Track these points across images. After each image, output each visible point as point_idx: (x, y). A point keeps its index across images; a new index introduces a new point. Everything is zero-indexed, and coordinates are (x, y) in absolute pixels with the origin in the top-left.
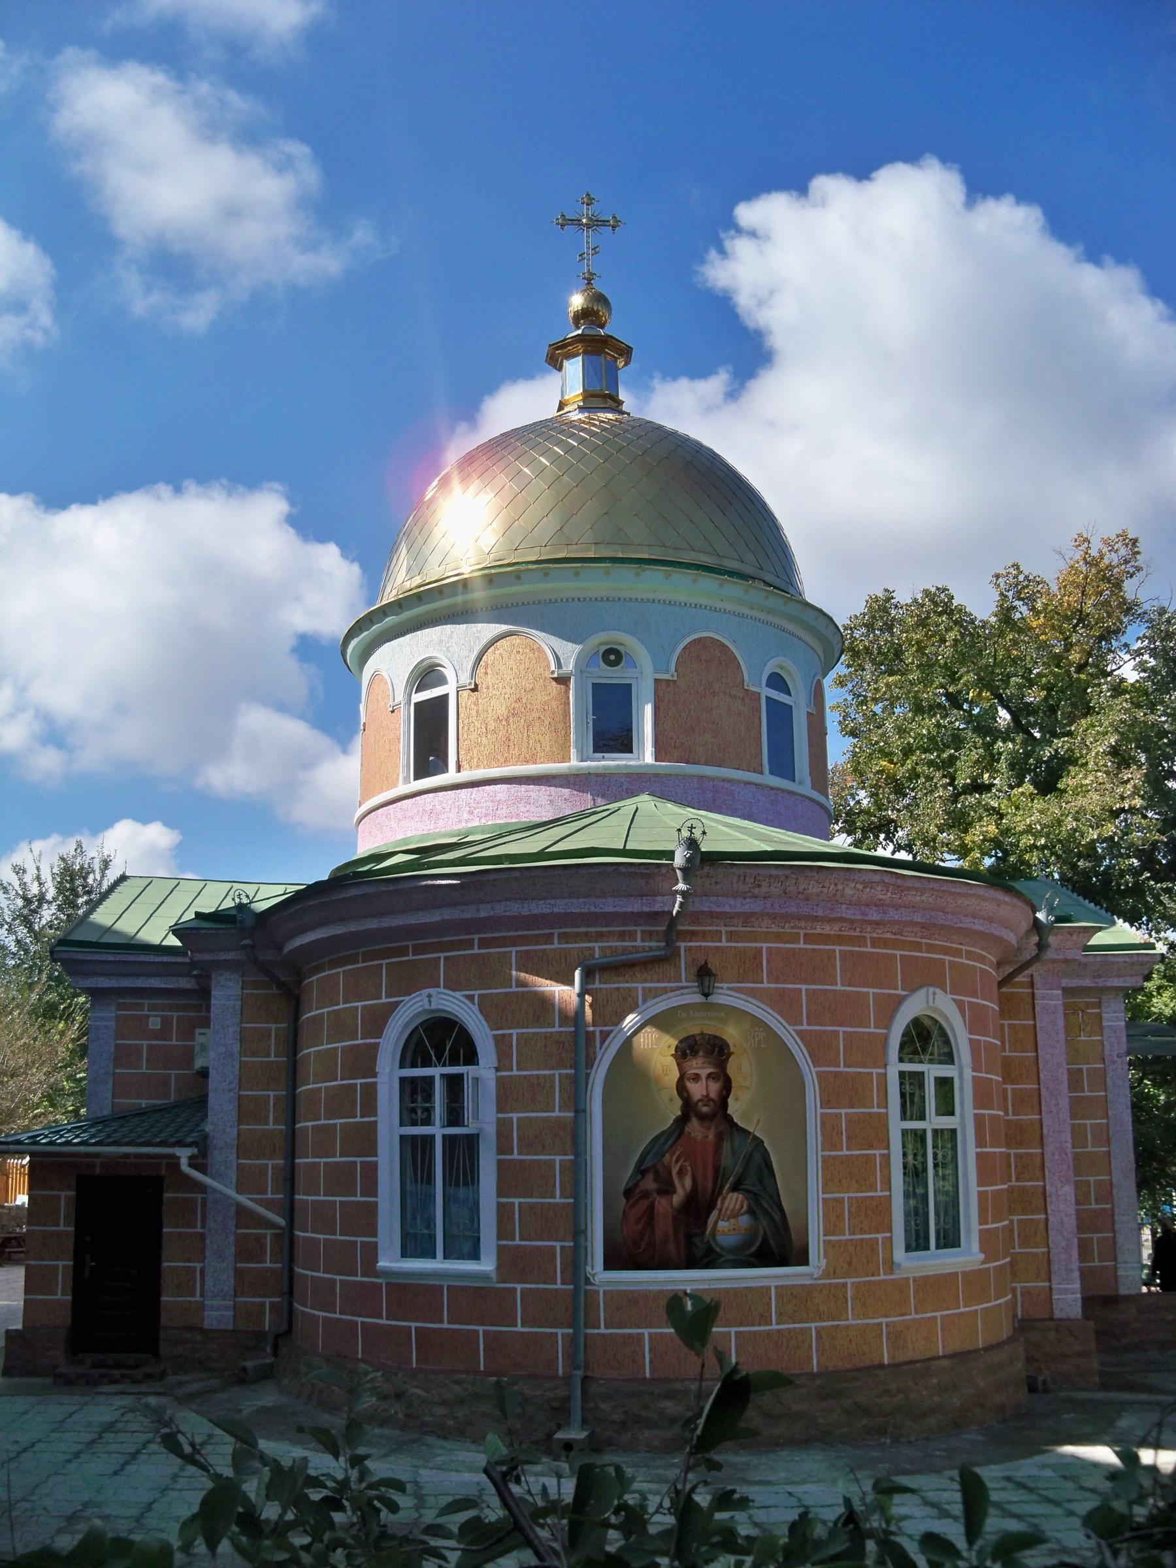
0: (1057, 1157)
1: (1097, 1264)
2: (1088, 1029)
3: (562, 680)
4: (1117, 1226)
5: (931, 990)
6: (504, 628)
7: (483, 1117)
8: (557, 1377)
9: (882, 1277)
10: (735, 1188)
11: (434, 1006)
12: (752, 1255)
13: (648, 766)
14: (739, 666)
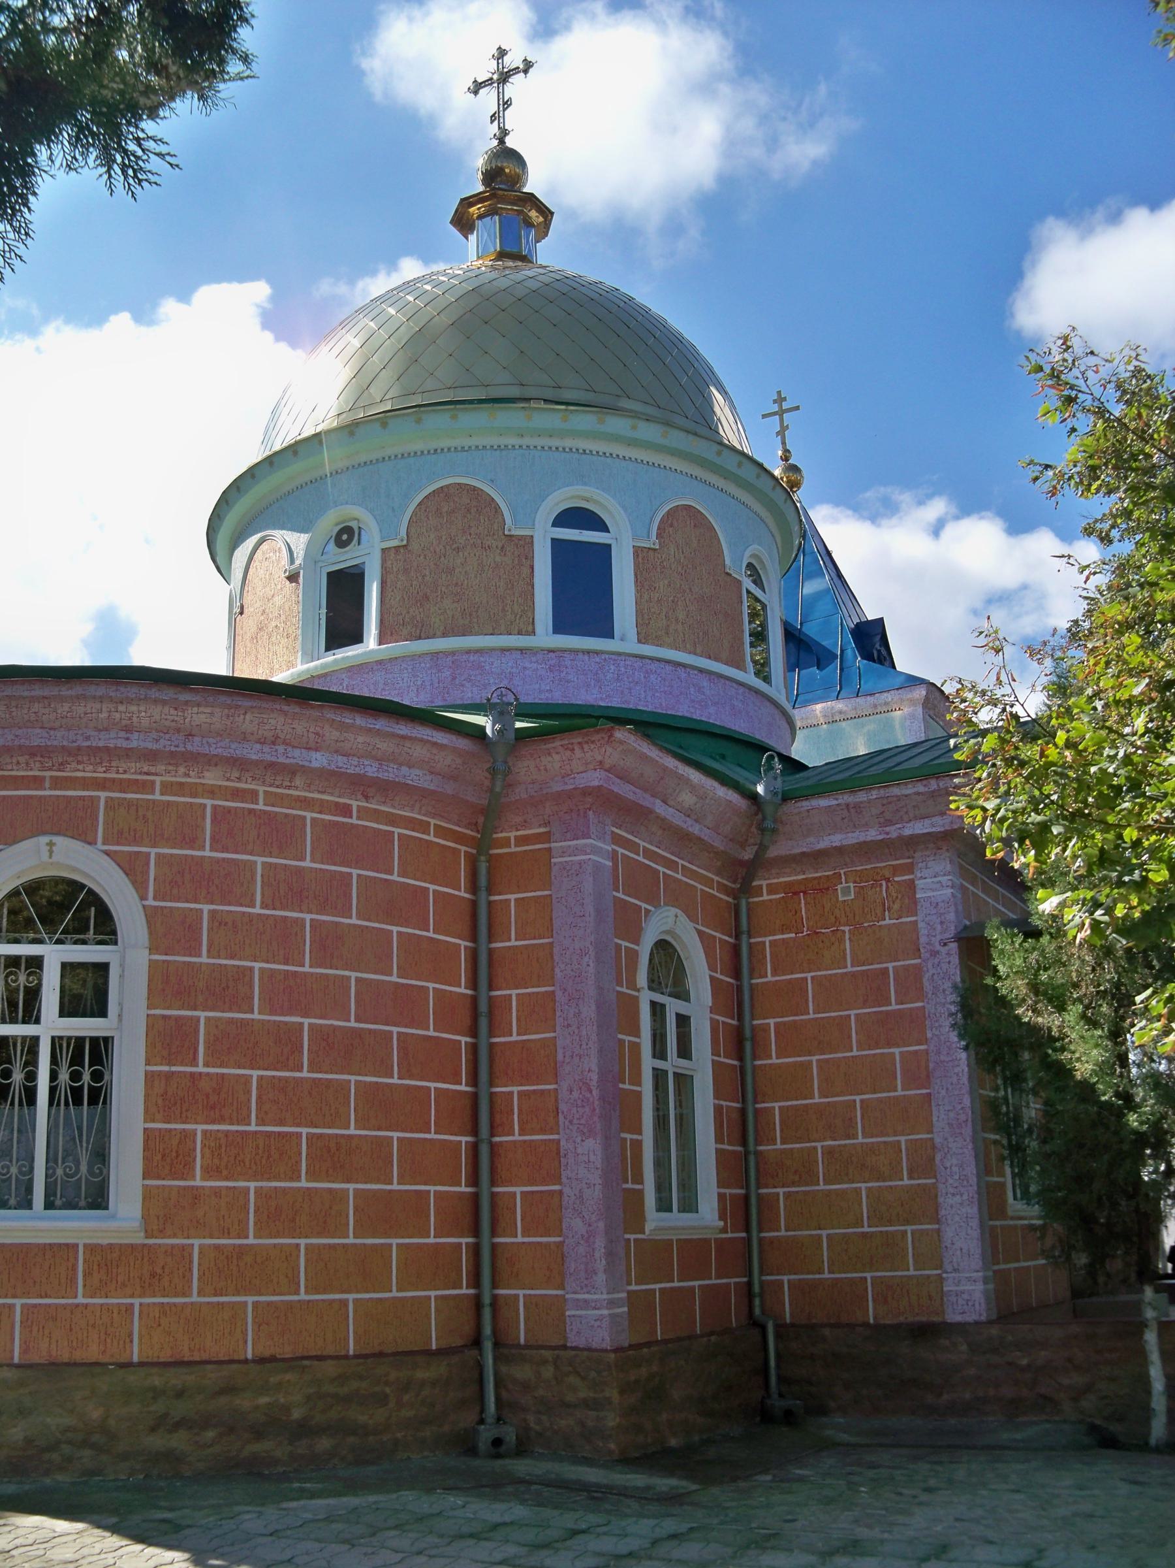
0: (576, 1094)
1: (912, 1272)
2: (896, 906)
3: (293, 578)
5: (44, 840)
6: (259, 536)
7: (127, 1022)
13: (372, 651)
14: (497, 509)
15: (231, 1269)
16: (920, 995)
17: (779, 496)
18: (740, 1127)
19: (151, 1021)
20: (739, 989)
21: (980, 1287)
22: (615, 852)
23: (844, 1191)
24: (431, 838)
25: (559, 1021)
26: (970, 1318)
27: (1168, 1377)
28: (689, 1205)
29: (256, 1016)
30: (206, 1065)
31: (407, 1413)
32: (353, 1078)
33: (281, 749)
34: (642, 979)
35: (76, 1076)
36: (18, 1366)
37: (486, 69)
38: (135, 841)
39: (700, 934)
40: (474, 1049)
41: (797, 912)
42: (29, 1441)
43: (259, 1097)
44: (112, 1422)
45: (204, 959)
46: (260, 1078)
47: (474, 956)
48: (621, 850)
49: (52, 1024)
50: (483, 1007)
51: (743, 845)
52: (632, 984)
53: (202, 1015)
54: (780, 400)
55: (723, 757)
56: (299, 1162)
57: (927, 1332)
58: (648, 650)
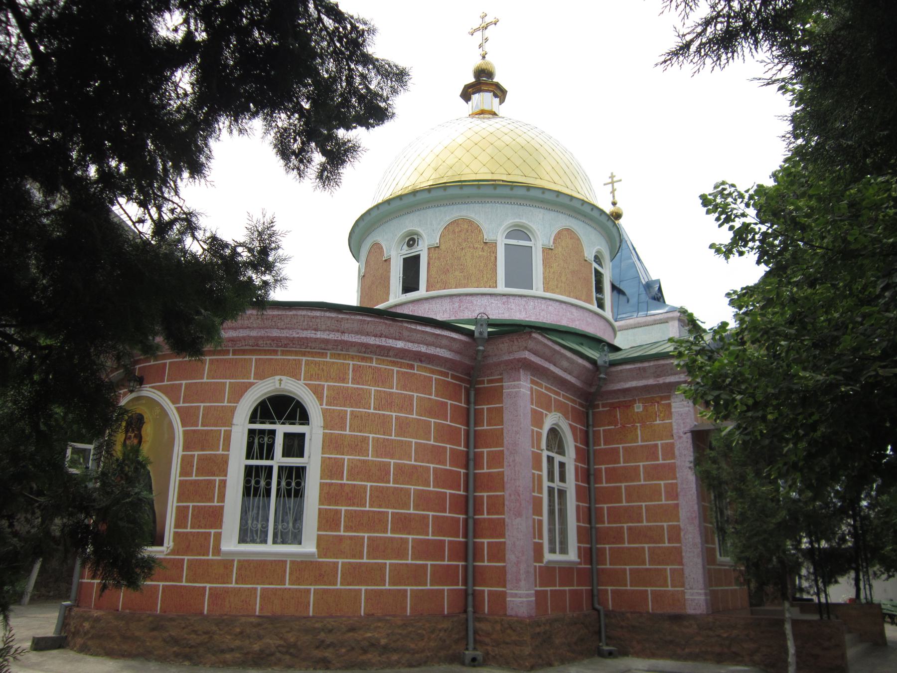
0: (513, 497)
4: (685, 560)
5: (278, 378)
7: (313, 459)
8: (202, 613)
9: (210, 557)
11: (282, 386)
15: (356, 574)
16: (673, 457)
17: (610, 224)
18: (588, 515)
19: (324, 460)
20: (588, 451)
21: (703, 598)
22: (532, 388)
23: (637, 548)
24: (449, 380)
25: (505, 464)
26: (698, 612)
27: (797, 647)
28: (564, 550)
29: (370, 458)
30: (347, 480)
31: (432, 644)
32: (412, 487)
33: (384, 339)
34: (544, 445)
35: (289, 484)
36: (259, 616)
37: (477, 23)
38: (318, 379)
39: (570, 425)
40: (467, 475)
41: (615, 416)
42: (262, 651)
43: (371, 495)
44: (299, 643)
45: (347, 432)
46: (371, 486)
47: (467, 433)
48: (534, 387)
49: (279, 460)
50: (471, 456)
51: (591, 385)
52: (539, 448)
53: (346, 457)
54: (612, 177)
55: (582, 344)
56: (387, 525)
57: (678, 618)
58: (548, 295)
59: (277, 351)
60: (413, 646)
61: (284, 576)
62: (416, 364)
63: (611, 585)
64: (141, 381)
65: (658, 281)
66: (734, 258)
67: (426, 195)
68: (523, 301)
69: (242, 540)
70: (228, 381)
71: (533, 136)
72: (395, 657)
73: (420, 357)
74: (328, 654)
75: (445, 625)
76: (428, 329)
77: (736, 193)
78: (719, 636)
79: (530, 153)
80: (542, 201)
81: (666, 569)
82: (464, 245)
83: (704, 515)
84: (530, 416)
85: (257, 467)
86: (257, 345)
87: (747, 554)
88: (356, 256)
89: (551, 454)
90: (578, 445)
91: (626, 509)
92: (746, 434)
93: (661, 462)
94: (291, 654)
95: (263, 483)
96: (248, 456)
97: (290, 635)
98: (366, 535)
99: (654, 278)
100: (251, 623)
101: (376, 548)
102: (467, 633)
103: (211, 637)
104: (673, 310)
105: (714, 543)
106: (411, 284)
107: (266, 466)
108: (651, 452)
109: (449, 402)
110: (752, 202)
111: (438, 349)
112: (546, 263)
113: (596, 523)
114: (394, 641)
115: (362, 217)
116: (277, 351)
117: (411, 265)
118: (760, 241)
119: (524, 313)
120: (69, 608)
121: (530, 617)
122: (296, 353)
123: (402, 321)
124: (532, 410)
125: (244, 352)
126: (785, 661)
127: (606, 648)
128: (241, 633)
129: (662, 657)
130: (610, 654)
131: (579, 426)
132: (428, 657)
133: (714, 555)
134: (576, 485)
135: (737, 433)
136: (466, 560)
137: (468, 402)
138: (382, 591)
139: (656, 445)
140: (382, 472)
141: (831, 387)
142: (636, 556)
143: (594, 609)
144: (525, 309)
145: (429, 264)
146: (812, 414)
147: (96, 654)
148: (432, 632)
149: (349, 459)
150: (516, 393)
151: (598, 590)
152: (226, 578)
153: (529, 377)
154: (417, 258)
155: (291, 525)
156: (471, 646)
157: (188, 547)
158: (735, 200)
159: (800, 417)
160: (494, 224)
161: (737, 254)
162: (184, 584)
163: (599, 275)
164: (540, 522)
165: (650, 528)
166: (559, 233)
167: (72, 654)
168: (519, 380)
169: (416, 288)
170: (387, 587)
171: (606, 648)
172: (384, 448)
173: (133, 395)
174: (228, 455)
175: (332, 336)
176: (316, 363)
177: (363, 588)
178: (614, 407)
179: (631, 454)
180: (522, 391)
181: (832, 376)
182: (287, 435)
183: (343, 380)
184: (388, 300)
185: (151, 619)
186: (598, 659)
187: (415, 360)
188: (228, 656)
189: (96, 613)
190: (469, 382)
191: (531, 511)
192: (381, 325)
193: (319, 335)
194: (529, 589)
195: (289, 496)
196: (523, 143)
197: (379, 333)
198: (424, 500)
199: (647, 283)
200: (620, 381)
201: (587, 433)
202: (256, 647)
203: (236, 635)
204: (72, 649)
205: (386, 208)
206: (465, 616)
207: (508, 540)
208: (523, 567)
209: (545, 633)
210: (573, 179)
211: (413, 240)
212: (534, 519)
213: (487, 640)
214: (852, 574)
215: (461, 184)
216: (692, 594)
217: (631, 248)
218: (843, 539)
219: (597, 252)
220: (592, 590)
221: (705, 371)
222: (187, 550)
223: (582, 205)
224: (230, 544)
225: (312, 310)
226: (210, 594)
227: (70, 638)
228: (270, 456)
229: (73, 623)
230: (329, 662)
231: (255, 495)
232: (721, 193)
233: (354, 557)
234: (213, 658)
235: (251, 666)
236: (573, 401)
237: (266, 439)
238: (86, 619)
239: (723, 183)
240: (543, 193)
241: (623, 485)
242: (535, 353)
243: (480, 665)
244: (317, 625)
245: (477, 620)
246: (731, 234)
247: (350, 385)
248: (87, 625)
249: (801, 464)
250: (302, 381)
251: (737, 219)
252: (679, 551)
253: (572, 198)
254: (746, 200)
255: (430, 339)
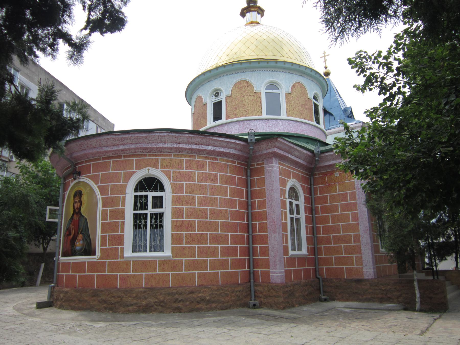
4: (362, 252)
5: (147, 168)
7: (167, 209)
8: (116, 288)
9: (119, 260)
10: (81, 233)
11: (150, 173)
12: (83, 252)
15: (192, 265)
18: (313, 231)
19: (173, 209)
20: (311, 198)
21: (372, 270)
22: (279, 167)
23: (338, 246)
24: (236, 165)
25: (267, 206)
26: (370, 278)
28: (300, 249)
29: (197, 207)
30: (185, 218)
31: (233, 298)
33: (200, 146)
34: (287, 196)
35: (156, 222)
38: (168, 168)
39: (301, 185)
40: (248, 213)
42: (147, 305)
43: (198, 226)
44: (165, 300)
45: (184, 194)
46: (198, 221)
49: (150, 210)
50: (250, 203)
51: (311, 164)
52: (284, 197)
54: (324, 53)
55: (308, 143)
57: (359, 281)
59: (146, 155)
60: (223, 300)
61: (156, 268)
62: (218, 158)
63: (325, 266)
64: (79, 174)
65: (350, 108)
66: (367, 92)
67: (223, 69)
68: (276, 122)
69: (134, 251)
70: (122, 171)
71: (279, 34)
72: (214, 305)
73: (220, 154)
74: (180, 305)
75: (239, 289)
76: (223, 139)
77: (367, 57)
78: (381, 289)
79: (277, 43)
80: (284, 68)
81: (353, 257)
82: (244, 94)
83: (372, 228)
84: (279, 182)
85: (140, 214)
86: (136, 152)
87: (393, 248)
88: (190, 103)
89: (291, 200)
90: (306, 195)
91: (332, 227)
92: (372, 187)
93: (349, 202)
94: (161, 306)
95: (143, 222)
96: (135, 210)
97: (160, 297)
98: (196, 246)
99: (348, 106)
100: (141, 291)
101: (202, 252)
102: (251, 293)
103: (122, 299)
104: (359, 122)
105: (378, 242)
106: (218, 116)
107: (144, 214)
108: (344, 197)
109: (237, 176)
110: (376, 61)
111: (229, 149)
112: (287, 101)
113: (317, 235)
114: (213, 298)
115: (191, 83)
116: (146, 155)
117: (217, 106)
118: (380, 82)
119: (277, 128)
120: (53, 287)
121: (282, 283)
122: (156, 155)
123: (209, 136)
124: (280, 178)
125: (129, 156)
126: (415, 301)
127: (323, 297)
128: (136, 296)
129: (352, 300)
130: (325, 300)
131: (306, 185)
132: (231, 305)
133: (379, 249)
134: (305, 216)
135: (368, 186)
136: (249, 256)
137: (247, 175)
138: (206, 273)
139: (347, 193)
140: (203, 214)
141: (416, 160)
142: (337, 251)
143: (317, 278)
144: (277, 126)
145: (226, 105)
146: (407, 174)
147: (67, 309)
148: (233, 292)
149: (186, 208)
150: (271, 170)
151: (319, 268)
152: (127, 270)
153: (278, 161)
154: (220, 102)
155: (158, 242)
156: (253, 298)
157: (108, 255)
158: (367, 60)
159: (402, 177)
160: (259, 82)
161: (368, 90)
162: (107, 273)
163: (316, 107)
164: (286, 235)
165: (344, 236)
166: (294, 85)
167: (55, 309)
168: (272, 163)
169: (220, 118)
170: (209, 271)
171: (323, 297)
172: (204, 201)
173: (76, 181)
174: (125, 209)
175: (174, 146)
176: (166, 160)
177: (196, 272)
178: (324, 174)
179: (333, 198)
180: (274, 169)
181: (416, 154)
182: (153, 197)
183: (181, 168)
184: (206, 125)
185: (92, 291)
186: (319, 303)
187: (218, 155)
188: (130, 308)
189: (66, 289)
190: (247, 165)
191: (281, 230)
192: (199, 139)
193: (167, 145)
194: (281, 269)
195: (157, 228)
196: (273, 38)
197: (198, 143)
198: (225, 227)
199: (344, 109)
200: (326, 161)
201: (310, 189)
202: (144, 303)
203: (134, 298)
204: (56, 307)
205: (203, 77)
206: (249, 284)
207: (270, 245)
208: (278, 258)
209: (290, 291)
210: (301, 56)
211: (218, 93)
212: (283, 234)
213: (261, 295)
214: (454, 255)
215: (241, 62)
216: (367, 269)
217: (336, 91)
218: (449, 237)
219: (315, 94)
220: (315, 268)
221: (350, 154)
222: (107, 257)
223: (306, 69)
224: (128, 253)
225: (162, 132)
226: (120, 278)
227: (54, 302)
228: (146, 208)
229: (55, 294)
230: (181, 309)
231: (139, 228)
232: (359, 57)
233: (191, 257)
234: (123, 309)
235: (142, 312)
236: (302, 173)
237: (143, 200)
238: (61, 292)
239: (360, 51)
240: (285, 64)
241: (330, 214)
242: (281, 149)
243: (258, 308)
244: (174, 291)
245: (255, 285)
246: (364, 79)
247: (184, 170)
248: (62, 295)
249: (402, 201)
250: (160, 169)
251: (367, 71)
252: (359, 247)
253: (300, 66)
254: (372, 60)
255: (225, 144)
